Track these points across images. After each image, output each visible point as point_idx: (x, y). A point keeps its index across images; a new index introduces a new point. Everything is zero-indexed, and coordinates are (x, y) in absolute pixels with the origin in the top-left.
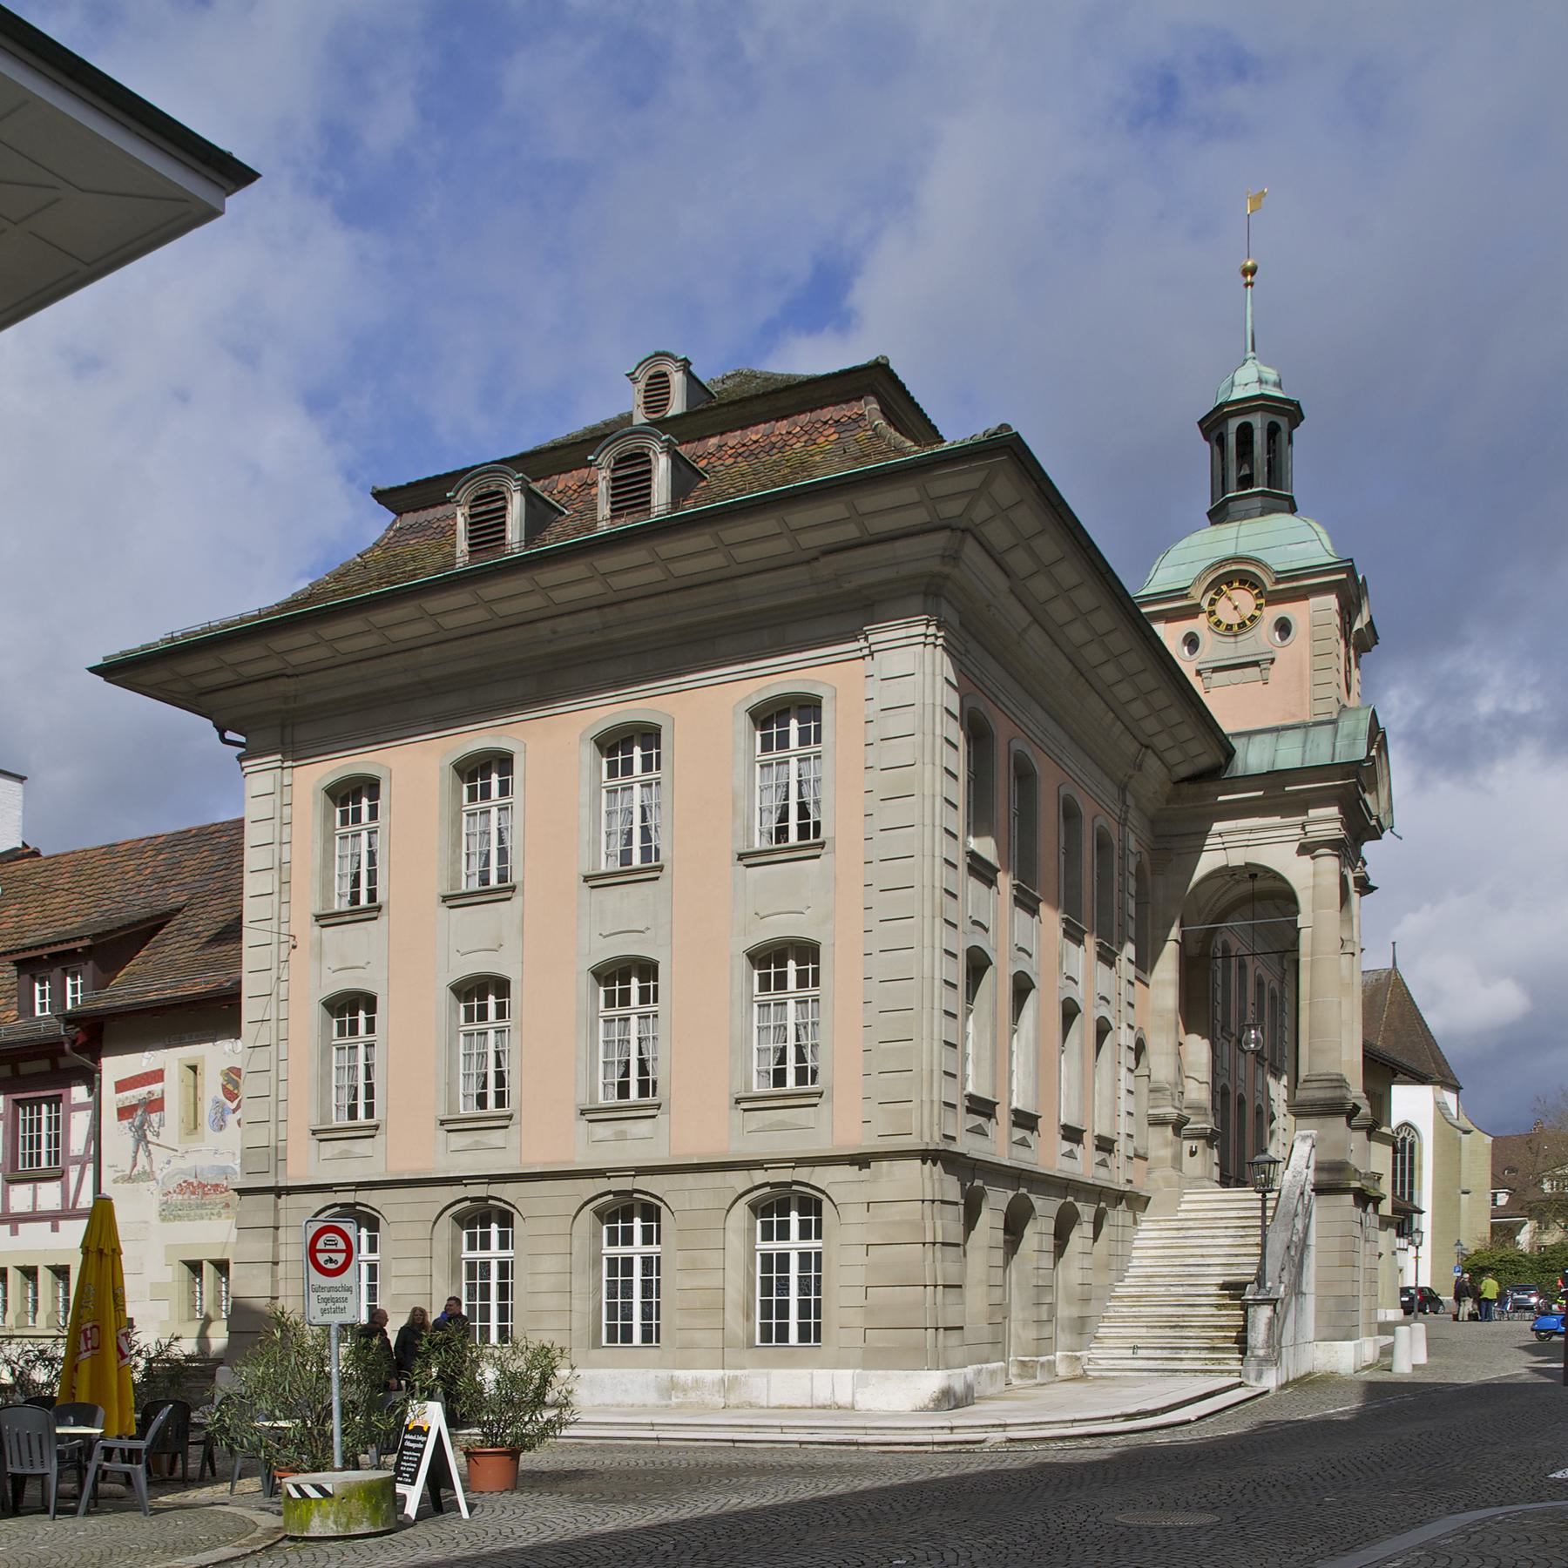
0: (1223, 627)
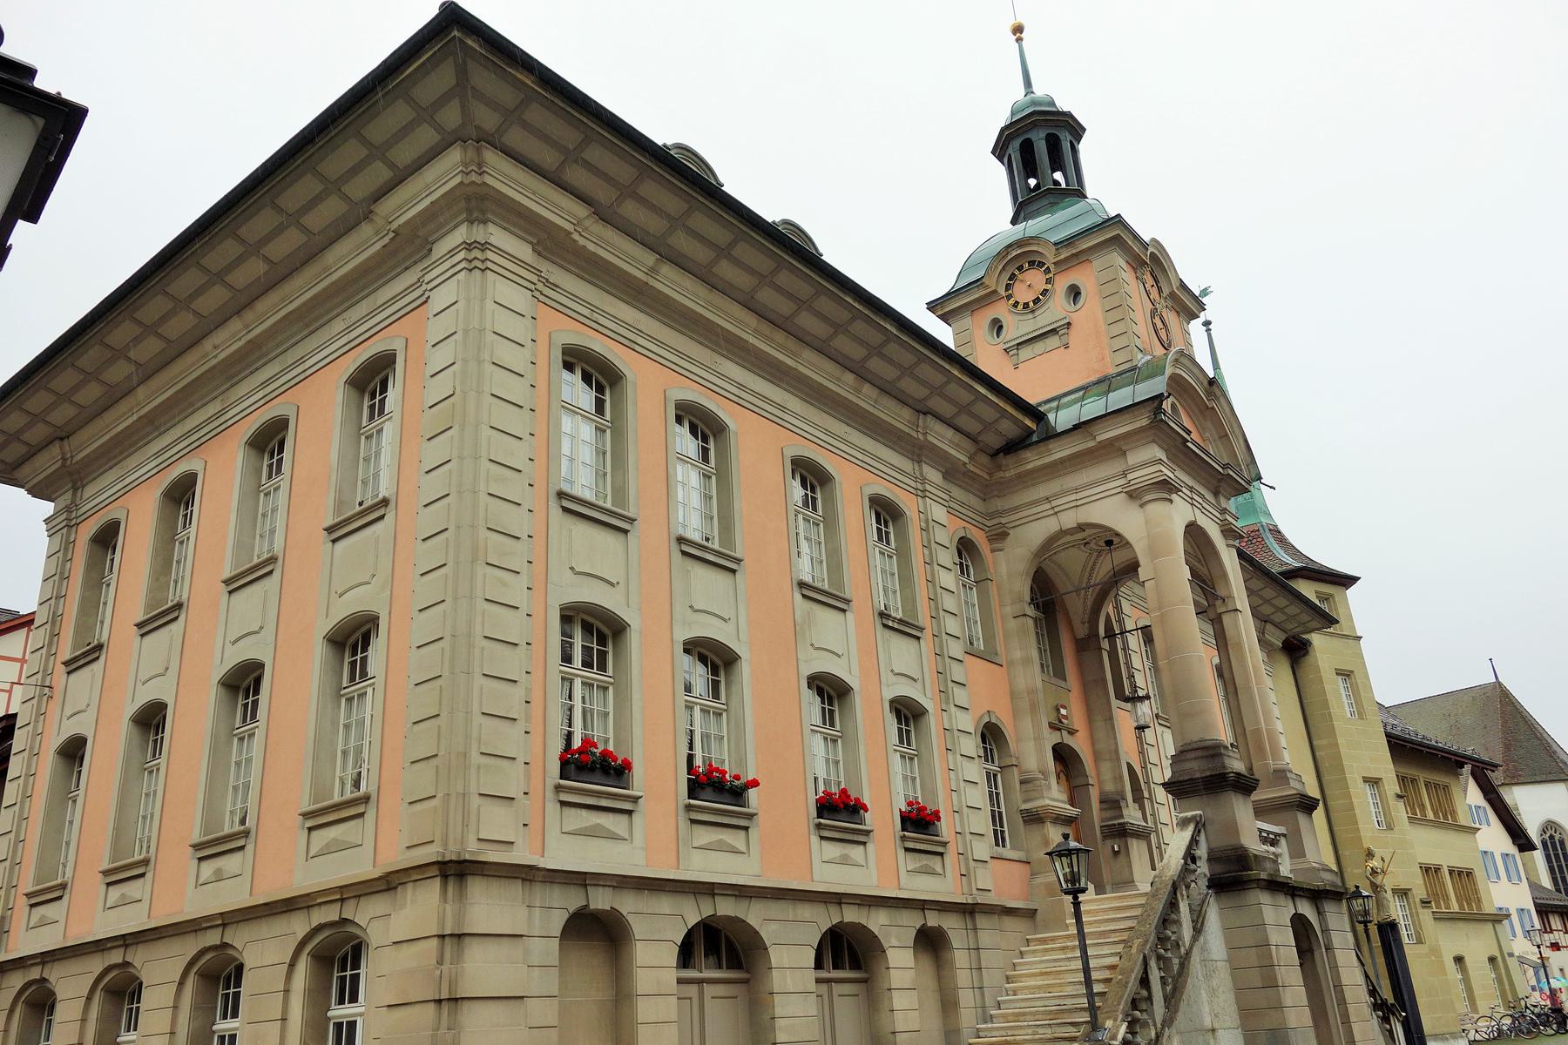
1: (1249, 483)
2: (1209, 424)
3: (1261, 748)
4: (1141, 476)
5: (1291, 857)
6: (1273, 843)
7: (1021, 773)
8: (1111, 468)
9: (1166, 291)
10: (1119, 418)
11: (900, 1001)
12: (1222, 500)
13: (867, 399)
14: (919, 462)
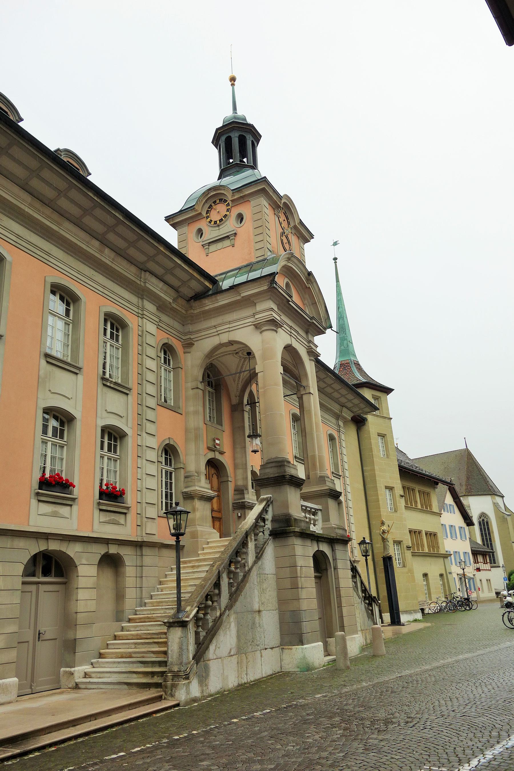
0: (212, 223)
1: (325, 329)
2: (307, 296)
3: (314, 465)
4: (262, 316)
5: (323, 521)
6: (314, 514)
7: (186, 472)
8: (248, 312)
9: (292, 225)
10: (251, 285)
11: (82, 595)
12: (310, 336)
13: (107, 257)
14: (142, 299)
